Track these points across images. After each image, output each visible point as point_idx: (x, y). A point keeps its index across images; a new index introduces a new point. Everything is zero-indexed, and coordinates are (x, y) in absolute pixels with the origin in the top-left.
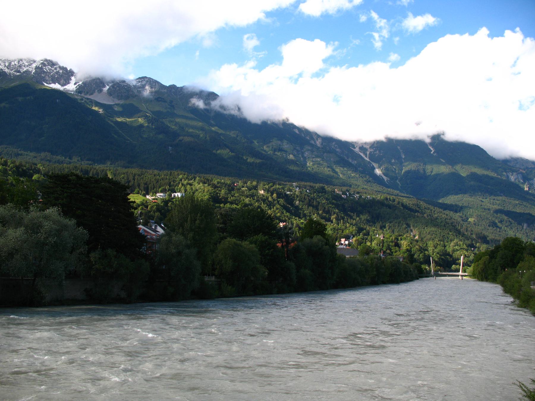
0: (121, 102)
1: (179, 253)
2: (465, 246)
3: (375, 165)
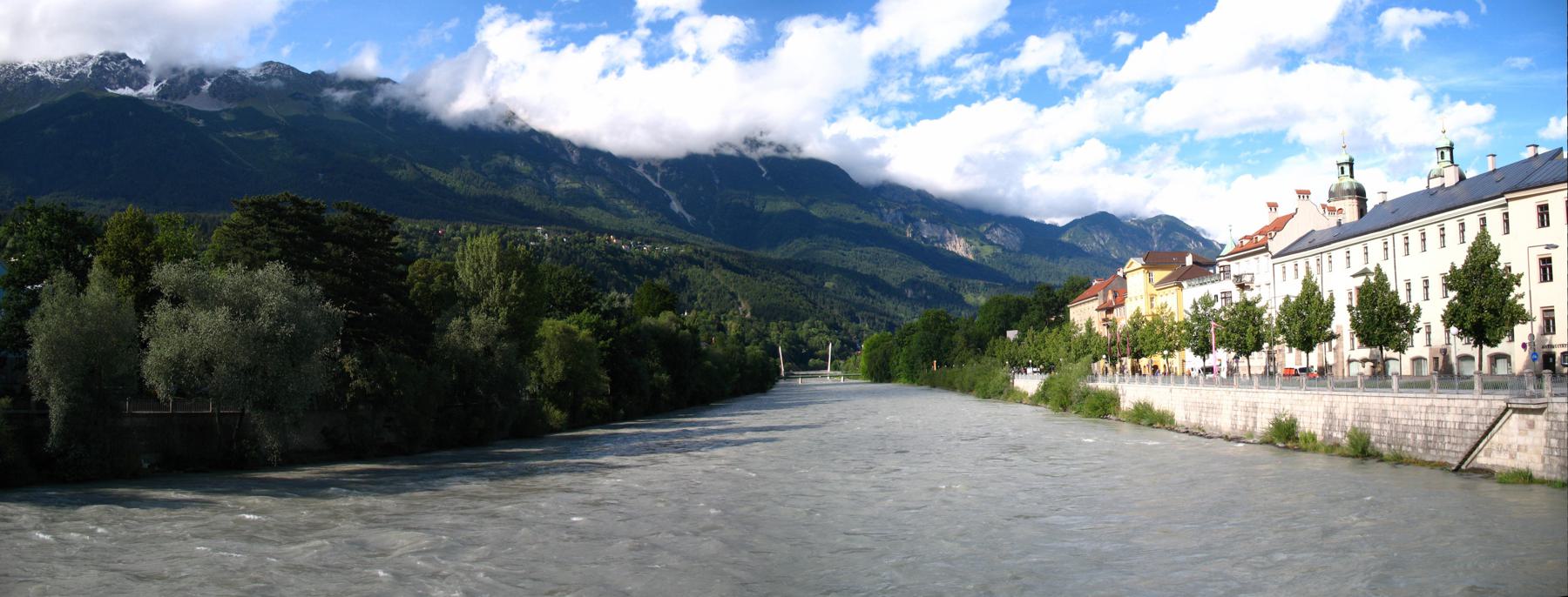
0: (233, 106)
1: (488, 351)
2: (825, 328)
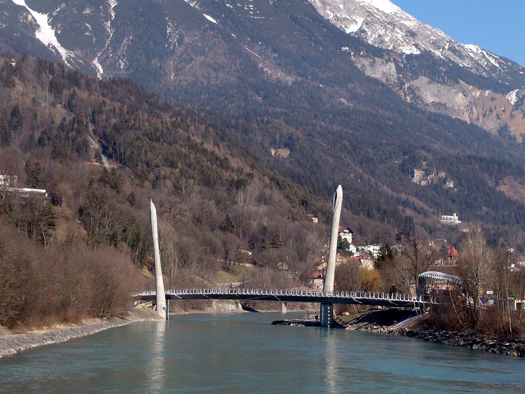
3: (42, 19)
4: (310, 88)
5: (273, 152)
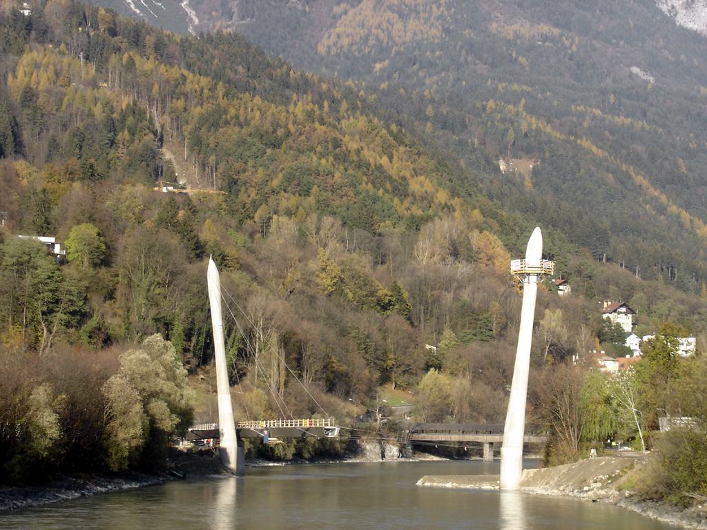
4: (574, 48)
5: (502, 167)
